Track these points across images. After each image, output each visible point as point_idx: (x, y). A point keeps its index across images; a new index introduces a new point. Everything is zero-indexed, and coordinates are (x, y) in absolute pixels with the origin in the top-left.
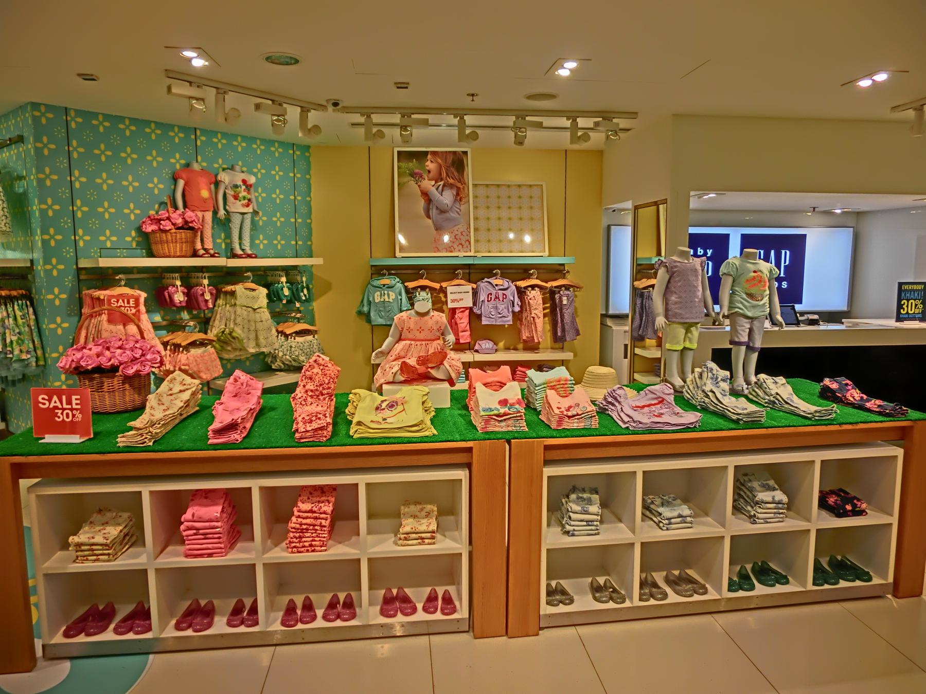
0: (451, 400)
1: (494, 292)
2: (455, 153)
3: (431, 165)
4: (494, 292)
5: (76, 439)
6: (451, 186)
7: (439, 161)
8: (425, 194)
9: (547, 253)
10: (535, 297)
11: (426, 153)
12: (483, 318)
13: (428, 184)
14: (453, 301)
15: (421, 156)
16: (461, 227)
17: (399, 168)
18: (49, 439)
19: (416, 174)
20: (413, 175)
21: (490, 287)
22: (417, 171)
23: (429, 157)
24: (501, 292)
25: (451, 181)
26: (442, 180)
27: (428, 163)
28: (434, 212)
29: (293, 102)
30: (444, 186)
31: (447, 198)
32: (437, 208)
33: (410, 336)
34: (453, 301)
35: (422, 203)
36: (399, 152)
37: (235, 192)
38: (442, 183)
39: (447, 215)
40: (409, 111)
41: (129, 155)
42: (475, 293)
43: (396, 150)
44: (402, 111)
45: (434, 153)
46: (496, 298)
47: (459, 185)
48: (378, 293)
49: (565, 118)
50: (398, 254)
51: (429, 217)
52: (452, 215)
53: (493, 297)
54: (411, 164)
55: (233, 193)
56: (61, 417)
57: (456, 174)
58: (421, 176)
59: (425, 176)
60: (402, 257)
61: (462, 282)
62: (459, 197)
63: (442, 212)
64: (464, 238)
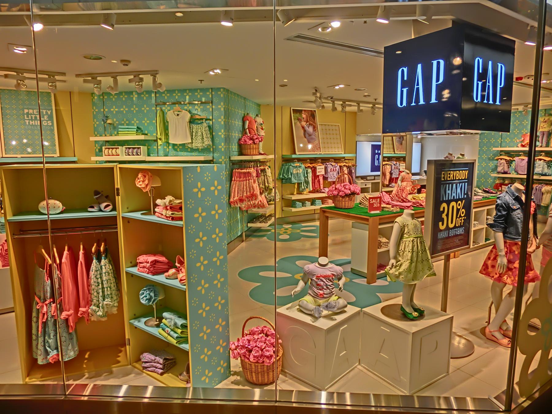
0: (252, 223)
1: (332, 168)
2: (311, 111)
3: (304, 116)
4: (332, 168)
5: (378, 212)
6: (311, 125)
7: (307, 114)
8: (303, 127)
9: (343, 153)
10: (346, 170)
11: (302, 110)
12: (329, 179)
13: (304, 123)
14: (319, 172)
15: (300, 112)
16: (317, 142)
17: (294, 116)
18: (373, 212)
19: (299, 119)
20: (299, 119)
21: (331, 166)
22: (299, 118)
23: (303, 112)
24: (334, 168)
25: (311, 122)
26: (308, 122)
27: (303, 115)
28: (307, 135)
29: (145, 72)
30: (309, 124)
31: (310, 130)
32: (308, 134)
33: (407, 180)
34: (319, 172)
35: (302, 131)
36: (293, 110)
37: (262, 126)
38: (308, 123)
39: (311, 137)
40: (138, 73)
41: (516, 131)
42: (326, 168)
43: (292, 108)
44: (135, 73)
45: (305, 111)
46: (334, 170)
47: (314, 124)
48: (295, 169)
49: (150, 75)
50: (297, 153)
51: (305, 137)
52: (313, 137)
53: (332, 170)
54: (297, 115)
55: (261, 127)
56: (375, 206)
57: (312, 119)
58: (301, 120)
59: (302, 120)
60: (22, 157)
61: (321, 164)
62: (314, 128)
63: (310, 135)
64: (318, 146)
